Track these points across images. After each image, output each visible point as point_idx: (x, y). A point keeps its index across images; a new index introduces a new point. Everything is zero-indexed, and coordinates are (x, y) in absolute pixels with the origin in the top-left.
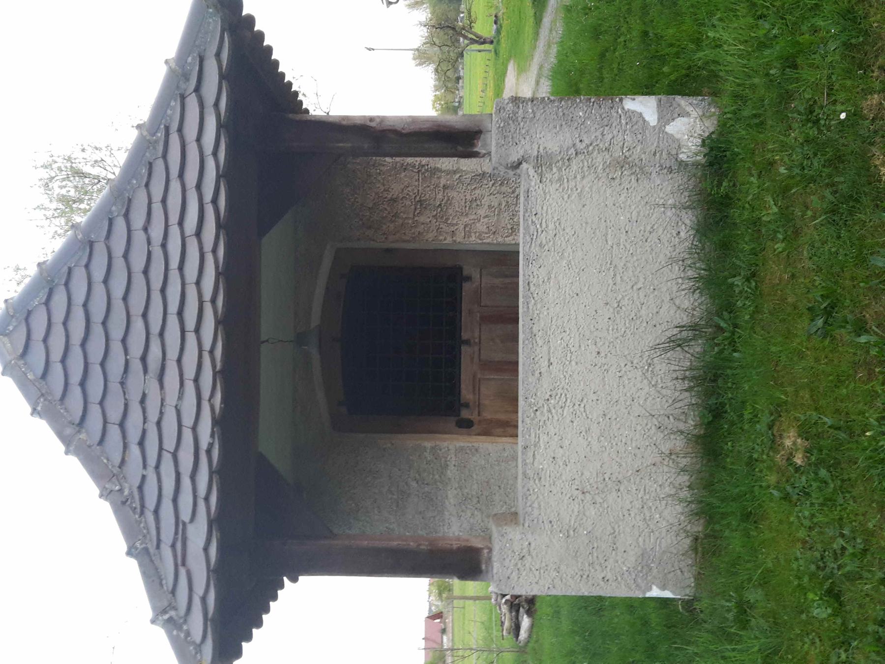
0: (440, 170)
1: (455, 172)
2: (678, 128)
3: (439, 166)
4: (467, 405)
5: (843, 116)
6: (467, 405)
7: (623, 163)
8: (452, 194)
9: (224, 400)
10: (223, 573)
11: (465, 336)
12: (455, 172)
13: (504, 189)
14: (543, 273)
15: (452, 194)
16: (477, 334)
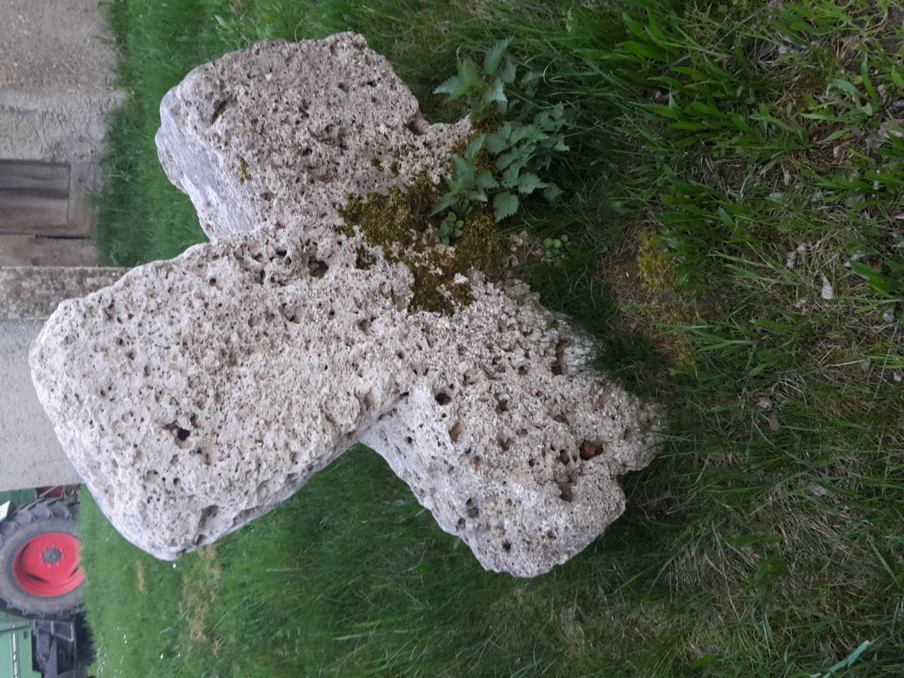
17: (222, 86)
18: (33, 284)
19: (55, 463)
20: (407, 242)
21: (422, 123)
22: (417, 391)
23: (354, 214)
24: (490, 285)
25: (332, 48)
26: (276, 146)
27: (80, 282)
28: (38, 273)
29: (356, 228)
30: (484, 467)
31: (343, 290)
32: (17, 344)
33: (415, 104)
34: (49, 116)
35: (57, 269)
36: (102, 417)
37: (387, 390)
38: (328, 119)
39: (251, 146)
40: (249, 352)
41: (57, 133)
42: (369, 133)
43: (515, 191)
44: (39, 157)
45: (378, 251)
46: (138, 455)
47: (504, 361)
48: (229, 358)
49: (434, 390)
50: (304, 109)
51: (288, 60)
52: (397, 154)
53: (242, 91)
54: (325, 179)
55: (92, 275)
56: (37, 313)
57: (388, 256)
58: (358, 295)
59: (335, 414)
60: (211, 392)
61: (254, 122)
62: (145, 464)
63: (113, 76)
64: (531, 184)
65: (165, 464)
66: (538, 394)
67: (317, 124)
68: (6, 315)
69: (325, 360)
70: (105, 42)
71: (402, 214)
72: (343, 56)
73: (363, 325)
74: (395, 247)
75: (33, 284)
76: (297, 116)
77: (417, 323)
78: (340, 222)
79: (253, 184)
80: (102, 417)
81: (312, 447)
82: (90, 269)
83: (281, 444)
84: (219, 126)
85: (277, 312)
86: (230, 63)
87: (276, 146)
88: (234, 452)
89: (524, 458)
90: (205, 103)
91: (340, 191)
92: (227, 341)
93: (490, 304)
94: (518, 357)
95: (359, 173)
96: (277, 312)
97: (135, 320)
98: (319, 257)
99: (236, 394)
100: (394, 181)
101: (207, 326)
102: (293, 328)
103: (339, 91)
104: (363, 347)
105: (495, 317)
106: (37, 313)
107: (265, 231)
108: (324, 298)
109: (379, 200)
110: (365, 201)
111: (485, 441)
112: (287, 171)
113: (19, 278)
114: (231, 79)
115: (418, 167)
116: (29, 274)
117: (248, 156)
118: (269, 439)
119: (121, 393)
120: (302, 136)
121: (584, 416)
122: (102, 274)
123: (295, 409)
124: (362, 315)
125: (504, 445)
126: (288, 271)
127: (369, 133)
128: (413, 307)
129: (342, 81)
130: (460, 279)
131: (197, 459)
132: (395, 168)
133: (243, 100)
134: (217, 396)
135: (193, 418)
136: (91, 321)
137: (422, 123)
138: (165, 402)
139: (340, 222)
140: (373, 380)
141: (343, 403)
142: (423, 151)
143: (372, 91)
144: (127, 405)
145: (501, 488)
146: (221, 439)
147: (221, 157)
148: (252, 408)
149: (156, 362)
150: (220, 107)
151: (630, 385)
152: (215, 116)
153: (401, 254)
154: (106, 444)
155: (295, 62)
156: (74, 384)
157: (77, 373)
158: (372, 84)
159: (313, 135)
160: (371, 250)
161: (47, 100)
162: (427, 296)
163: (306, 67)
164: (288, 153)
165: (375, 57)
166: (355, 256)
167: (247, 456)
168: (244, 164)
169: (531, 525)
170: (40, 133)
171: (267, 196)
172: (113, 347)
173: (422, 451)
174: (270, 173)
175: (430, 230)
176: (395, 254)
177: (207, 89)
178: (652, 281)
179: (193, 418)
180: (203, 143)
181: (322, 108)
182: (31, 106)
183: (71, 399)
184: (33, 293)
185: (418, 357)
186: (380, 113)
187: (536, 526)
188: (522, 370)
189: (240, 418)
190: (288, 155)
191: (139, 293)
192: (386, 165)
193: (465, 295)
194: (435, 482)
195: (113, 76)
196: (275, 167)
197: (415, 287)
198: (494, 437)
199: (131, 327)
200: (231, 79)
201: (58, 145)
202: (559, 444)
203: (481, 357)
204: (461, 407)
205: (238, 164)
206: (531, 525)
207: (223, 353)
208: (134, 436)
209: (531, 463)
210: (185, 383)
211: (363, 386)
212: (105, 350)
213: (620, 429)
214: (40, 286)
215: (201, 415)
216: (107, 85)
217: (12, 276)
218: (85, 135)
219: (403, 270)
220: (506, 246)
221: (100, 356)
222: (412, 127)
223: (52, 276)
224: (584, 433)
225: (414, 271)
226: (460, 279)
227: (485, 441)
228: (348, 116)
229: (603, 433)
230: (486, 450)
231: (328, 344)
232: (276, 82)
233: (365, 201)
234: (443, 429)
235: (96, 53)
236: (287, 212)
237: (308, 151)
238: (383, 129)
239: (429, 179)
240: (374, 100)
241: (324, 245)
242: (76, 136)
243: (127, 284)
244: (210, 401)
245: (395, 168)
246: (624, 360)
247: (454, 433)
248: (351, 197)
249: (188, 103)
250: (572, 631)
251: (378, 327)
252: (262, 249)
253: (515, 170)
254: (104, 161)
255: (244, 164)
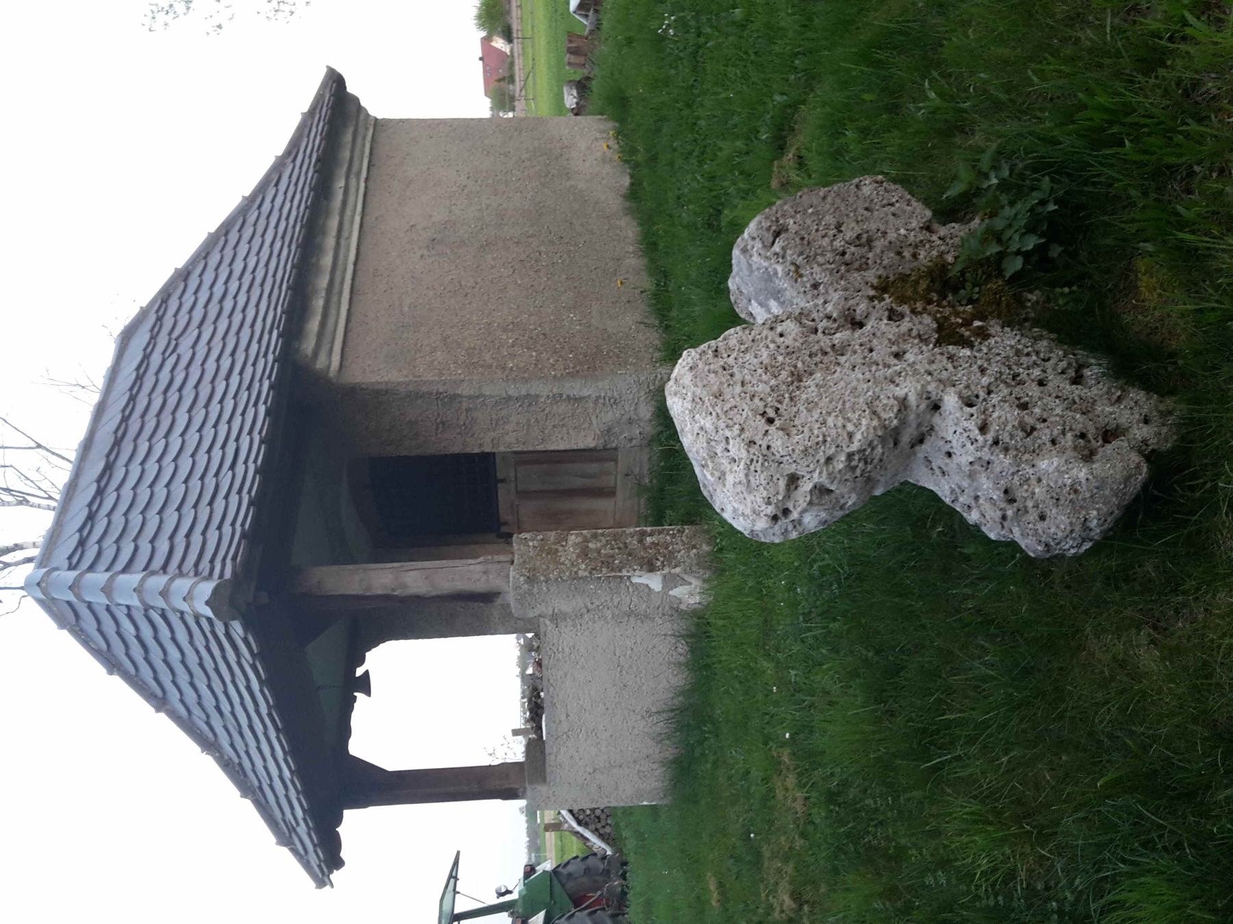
0: (459, 396)
1: (477, 397)
2: (678, 592)
3: (459, 392)
4: (505, 524)
5: (787, 735)
6: (505, 524)
7: (630, 613)
8: (475, 415)
9: (274, 696)
10: (311, 812)
11: (500, 476)
12: (477, 397)
13: (532, 409)
14: (560, 673)
15: (475, 415)
16: (512, 474)
17: (777, 221)
18: (599, 545)
19: (615, 771)
20: (930, 302)
21: (935, 226)
22: (946, 398)
23: (883, 288)
24: (1007, 329)
25: (857, 186)
26: (819, 251)
27: (641, 541)
28: (603, 535)
29: (886, 296)
30: (1012, 452)
31: (878, 334)
32: (586, 607)
33: (929, 213)
34: (601, 401)
35: (619, 530)
36: (718, 409)
37: (920, 396)
38: (858, 230)
39: (801, 254)
40: (811, 374)
41: (609, 416)
42: (892, 236)
43: (1018, 253)
44: (592, 445)
45: (905, 309)
46: (742, 430)
47: (1023, 376)
48: (797, 377)
49: (960, 397)
50: (838, 227)
51: (824, 198)
52: (916, 246)
53: (792, 222)
54: (859, 269)
55: (651, 535)
56: (604, 570)
57: (913, 311)
58: (891, 336)
59: (879, 410)
60: (787, 395)
61: (803, 239)
62: (747, 435)
63: (657, 355)
64: (1031, 242)
65: (760, 436)
66: (1057, 397)
67: (849, 235)
68: (576, 573)
69: (868, 375)
70: (647, 325)
71: (923, 285)
72: (866, 190)
73: (897, 356)
74: (919, 306)
75: (599, 545)
76: (835, 231)
77: (942, 354)
78: (872, 293)
79: (805, 279)
80: (718, 409)
81: (863, 428)
82: (649, 529)
83: (839, 424)
84: (777, 248)
85: (829, 350)
86: (781, 206)
87: (819, 251)
88: (806, 429)
89: (1046, 438)
90: (765, 233)
91: (871, 276)
92: (795, 367)
93: (1004, 340)
94: (1036, 372)
95: (885, 262)
96: (829, 350)
97: (732, 357)
98: (858, 318)
99: (804, 396)
100: (915, 264)
101: (780, 358)
102: (842, 359)
103: (865, 212)
104: (898, 368)
105: (1012, 347)
106: (604, 570)
107: (816, 305)
108: (864, 340)
109: (903, 278)
110: (892, 279)
111: (1009, 427)
112: (828, 266)
113: (586, 540)
114: (783, 216)
115: (935, 253)
116: (595, 536)
117: (800, 260)
118: (830, 421)
119: (727, 397)
120: (838, 244)
121: (1104, 409)
122: (660, 533)
123: (848, 405)
124: (895, 348)
125: (1030, 431)
126: (835, 325)
127: (892, 236)
128: (938, 343)
129: (867, 205)
130: (977, 323)
131: (781, 433)
132: (915, 256)
133: (793, 227)
134: (791, 399)
135: (777, 410)
136: (704, 358)
137: (935, 226)
138: (756, 400)
139: (872, 293)
140: (909, 388)
141: (885, 402)
142: (939, 242)
143: (892, 209)
144: (733, 402)
145: (1031, 471)
146: (796, 422)
147: (779, 269)
148: (816, 404)
149: (748, 378)
150: (777, 234)
151: (1148, 386)
152: (773, 243)
153: (925, 309)
154: (722, 425)
155: (829, 199)
156: (698, 391)
157: (700, 384)
158: (892, 205)
159: (847, 243)
160: (899, 309)
161: (600, 384)
162: (947, 335)
163: (838, 201)
164: (829, 255)
165: (893, 187)
166: (886, 313)
167: (816, 432)
168: (797, 267)
169: (1056, 482)
170: (593, 418)
171: (815, 286)
172: (720, 370)
173: (964, 471)
174: (816, 268)
175: (950, 297)
176: (919, 309)
177: (766, 224)
178: (1156, 301)
179: (777, 410)
180: (766, 264)
181: (853, 224)
182: (585, 393)
183: (697, 400)
184: (599, 552)
185: (945, 375)
186: (899, 222)
187: (1060, 482)
188: (1041, 383)
189: (809, 410)
190: (829, 256)
191: (733, 342)
192: (907, 254)
193: (984, 334)
194: (975, 484)
195: (657, 355)
196: (820, 265)
197: (940, 329)
198: (1016, 423)
199: (731, 361)
200: (783, 216)
201: (609, 430)
202: (1079, 427)
203: (1001, 373)
204: (986, 410)
205: (793, 268)
206: (1056, 482)
207: (792, 374)
208: (738, 419)
209: (1053, 442)
210: (768, 390)
211: (900, 392)
212: (716, 372)
213: (1138, 417)
214: (605, 546)
215: (782, 408)
216: (653, 363)
217: (580, 539)
218: (634, 417)
219: (927, 319)
220: (1020, 302)
221: (713, 375)
222: (928, 228)
223: (616, 537)
224: (1102, 421)
225: (937, 320)
226: (977, 323)
227: (1009, 427)
228: (873, 227)
229: (1122, 420)
230: (1012, 436)
231: (870, 367)
232: (816, 213)
233: (892, 279)
234: (972, 425)
235: (640, 336)
236: (831, 291)
237: (843, 254)
238: (902, 231)
239: (945, 260)
240: (894, 215)
241: (862, 307)
242: (626, 417)
243: (725, 339)
244: (787, 400)
245: (915, 256)
246: (1135, 364)
247: (983, 429)
248: (880, 277)
249: (753, 239)
250: (1148, 658)
251: (910, 357)
252: (815, 315)
253: (1016, 237)
254: (651, 442)
255: (797, 267)
